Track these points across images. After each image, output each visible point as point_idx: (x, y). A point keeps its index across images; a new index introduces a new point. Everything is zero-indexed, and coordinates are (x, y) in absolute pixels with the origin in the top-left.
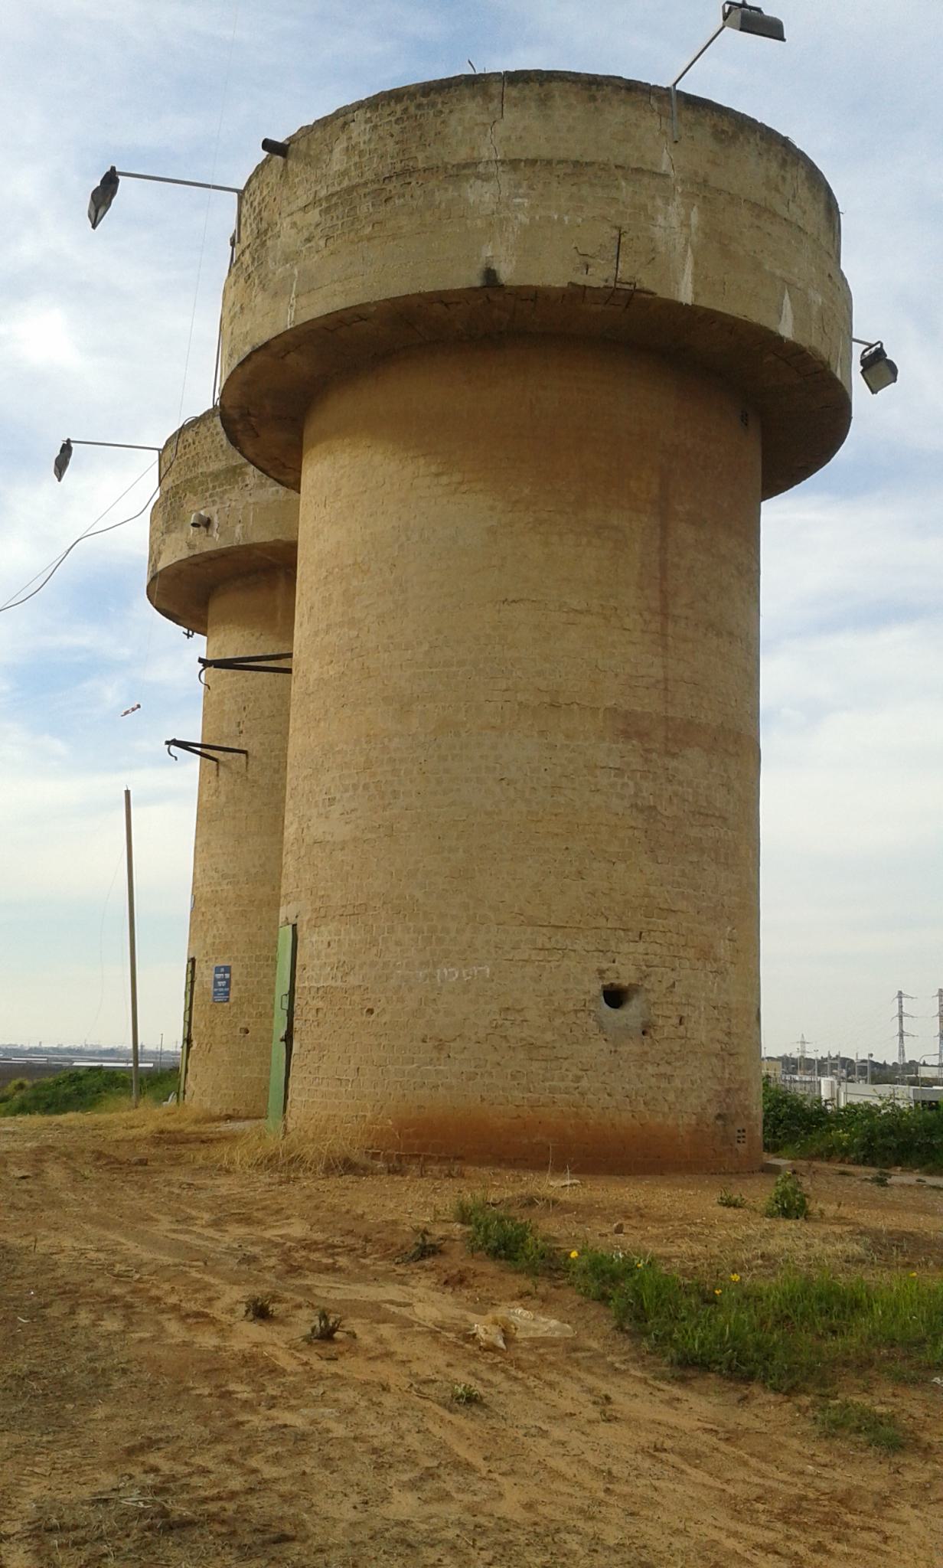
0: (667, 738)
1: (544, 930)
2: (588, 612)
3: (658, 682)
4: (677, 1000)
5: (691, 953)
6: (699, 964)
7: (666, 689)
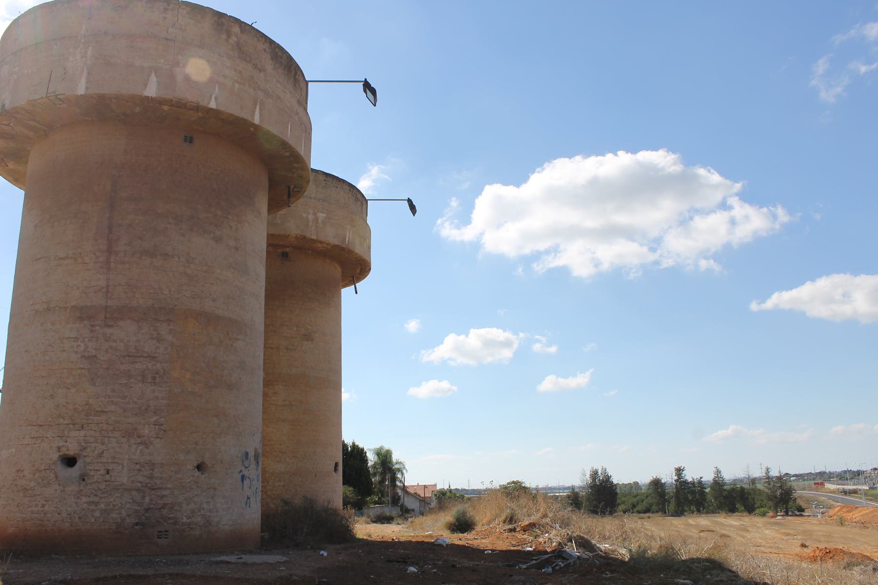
0: (106, 318)
1: (35, 428)
2: (67, 258)
3: (102, 288)
4: (104, 460)
5: (117, 434)
6: (124, 440)
7: (107, 291)
